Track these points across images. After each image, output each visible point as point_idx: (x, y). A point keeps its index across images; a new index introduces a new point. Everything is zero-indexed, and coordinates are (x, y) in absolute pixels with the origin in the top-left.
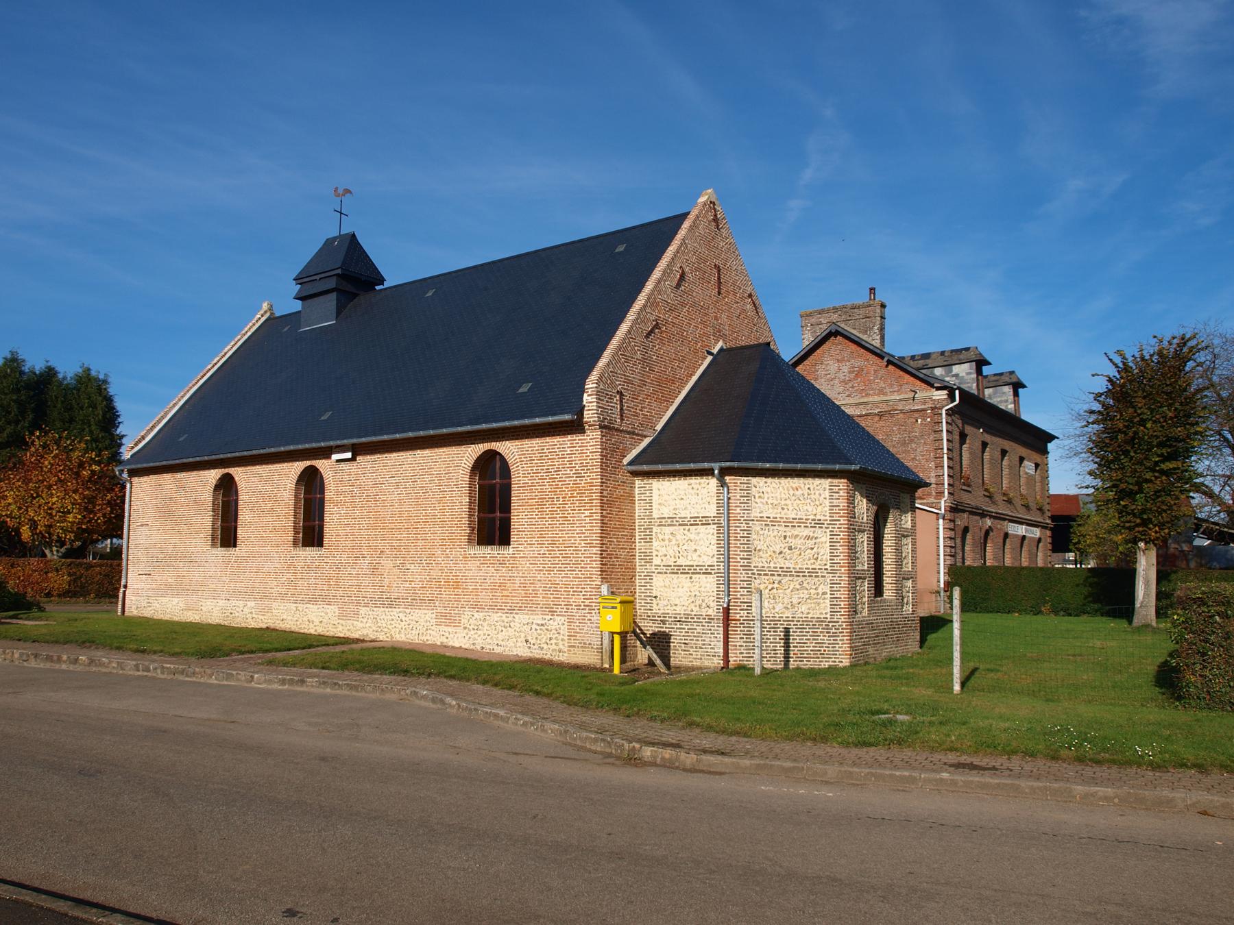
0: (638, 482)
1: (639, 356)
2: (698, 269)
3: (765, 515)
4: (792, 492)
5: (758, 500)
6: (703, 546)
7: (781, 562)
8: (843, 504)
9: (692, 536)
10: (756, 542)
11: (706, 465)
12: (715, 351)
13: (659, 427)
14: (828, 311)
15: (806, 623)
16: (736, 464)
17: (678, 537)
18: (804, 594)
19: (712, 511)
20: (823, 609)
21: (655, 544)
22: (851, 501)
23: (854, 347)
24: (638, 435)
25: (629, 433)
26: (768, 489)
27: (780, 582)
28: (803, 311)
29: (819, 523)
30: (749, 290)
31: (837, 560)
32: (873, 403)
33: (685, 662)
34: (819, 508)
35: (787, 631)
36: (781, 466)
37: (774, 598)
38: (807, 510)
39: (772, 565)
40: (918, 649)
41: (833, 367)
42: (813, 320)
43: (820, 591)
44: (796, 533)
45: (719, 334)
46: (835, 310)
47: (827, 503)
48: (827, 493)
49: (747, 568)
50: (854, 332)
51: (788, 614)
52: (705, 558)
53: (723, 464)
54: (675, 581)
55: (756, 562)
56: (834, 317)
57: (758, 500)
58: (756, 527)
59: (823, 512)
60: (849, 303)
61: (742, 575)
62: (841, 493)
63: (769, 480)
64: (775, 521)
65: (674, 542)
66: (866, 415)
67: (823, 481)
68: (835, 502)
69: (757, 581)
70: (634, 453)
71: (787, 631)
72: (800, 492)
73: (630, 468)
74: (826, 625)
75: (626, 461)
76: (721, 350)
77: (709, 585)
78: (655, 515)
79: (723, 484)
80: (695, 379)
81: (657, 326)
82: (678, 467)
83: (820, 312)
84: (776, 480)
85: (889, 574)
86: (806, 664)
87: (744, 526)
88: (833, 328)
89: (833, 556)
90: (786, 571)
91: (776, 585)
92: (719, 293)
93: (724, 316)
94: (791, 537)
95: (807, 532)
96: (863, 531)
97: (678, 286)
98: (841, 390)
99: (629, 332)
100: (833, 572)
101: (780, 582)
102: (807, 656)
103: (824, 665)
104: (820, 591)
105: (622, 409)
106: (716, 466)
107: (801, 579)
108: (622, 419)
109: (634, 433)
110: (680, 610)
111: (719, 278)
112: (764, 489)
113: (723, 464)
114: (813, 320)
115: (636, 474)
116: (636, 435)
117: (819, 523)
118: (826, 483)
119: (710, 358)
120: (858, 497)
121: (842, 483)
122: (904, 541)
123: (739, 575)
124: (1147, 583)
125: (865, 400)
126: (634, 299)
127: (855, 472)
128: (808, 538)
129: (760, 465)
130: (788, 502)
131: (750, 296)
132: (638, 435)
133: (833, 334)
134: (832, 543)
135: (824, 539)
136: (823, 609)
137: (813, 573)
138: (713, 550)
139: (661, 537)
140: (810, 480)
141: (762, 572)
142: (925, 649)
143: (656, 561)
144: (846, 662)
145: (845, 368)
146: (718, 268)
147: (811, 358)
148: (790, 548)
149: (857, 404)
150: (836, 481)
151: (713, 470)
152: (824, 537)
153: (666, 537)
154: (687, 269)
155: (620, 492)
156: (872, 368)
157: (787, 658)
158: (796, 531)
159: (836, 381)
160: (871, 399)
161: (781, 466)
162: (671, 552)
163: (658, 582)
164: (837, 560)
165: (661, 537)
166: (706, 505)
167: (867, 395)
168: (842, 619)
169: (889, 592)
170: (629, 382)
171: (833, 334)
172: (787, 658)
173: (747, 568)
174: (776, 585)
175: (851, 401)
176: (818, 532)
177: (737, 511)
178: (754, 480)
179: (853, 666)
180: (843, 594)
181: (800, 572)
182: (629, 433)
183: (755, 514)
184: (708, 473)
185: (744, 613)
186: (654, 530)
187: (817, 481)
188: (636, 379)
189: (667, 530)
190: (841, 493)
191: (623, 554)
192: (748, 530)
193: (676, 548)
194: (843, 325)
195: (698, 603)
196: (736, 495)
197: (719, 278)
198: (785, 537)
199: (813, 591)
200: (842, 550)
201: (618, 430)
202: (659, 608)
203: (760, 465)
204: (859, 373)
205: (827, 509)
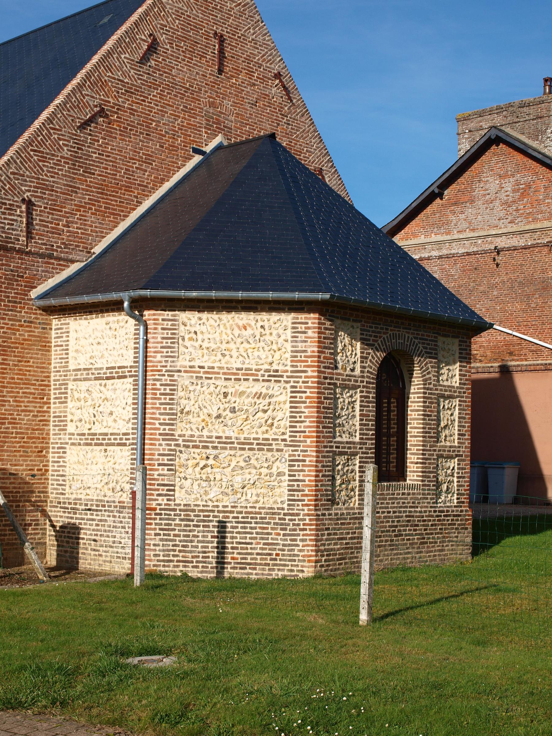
0: (55, 322)
1: (66, 152)
2: (184, 39)
3: (197, 363)
4: (237, 332)
5: (187, 343)
6: (117, 406)
7: (218, 430)
8: (312, 348)
9: (109, 394)
10: (183, 402)
11: (114, 296)
12: (208, 149)
13: (98, 249)
14: (491, 112)
15: (249, 516)
16: (148, 293)
17: (95, 395)
18: (250, 475)
19: (127, 358)
20: (279, 496)
21: (70, 404)
22: (327, 346)
23: (519, 157)
24: (58, 259)
25: (42, 256)
26: (203, 328)
27: (216, 457)
28: (459, 115)
29: (275, 376)
30: (276, 68)
31: (300, 427)
32: (542, 230)
33: (96, 567)
34: (277, 355)
35: (222, 526)
36: (213, 294)
37: (208, 480)
38: (260, 358)
39: (205, 433)
40: (463, 553)
41: (493, 184)
42: (472, 125)
43: (274, 470)
44: (241, 389)
45: (216, 125)
46: (500, 110)
47: (288, 346)
48: (289, 333)
49: (169, 437)
50: (523, 138)
51: (227, 501)
52: (121, 423)
53: (133, 293)
54: (90, 455)
55: (182, 428)
56: (498, 120)
57: (187, 343)
58: (184, 380)
59: (283, 360)
60: (517, 100)
61: (162, 447)
62: (310, 333)
63: (205, 315)
64: (210, 373)
65: (90, 402)
66: (533, 246)
67: (283, 316)
68: (301, 346)
69: (184, 456)
70: (51, 283)
71: (222, 526)
72: (249, 331)
73: (41, 303)
74: (281, 519)
75: (34, 294)
76: (219, 147)
77: (123, 458)
78: (71, 367)
79: (139, 319)
80: (167, 186)
81: (102, 113)
82: (86, 299)
83: (481, 114)
84: (215, 316)
85: (414, 450)
86: (238, 574)
87: (166, 379)
88: (493, 134)
89: (294, 421)
90: (226, 443)
91: (211, 462)
92: (220, 71)
93: (228, 104)
94: (234, 394)
95: (258, 387)
96: (355, 388)
97: (144, 59)
98: (502, 214)
99: (49, 120)
100: (294, 444)
101: (216, 457)
102: (250, 562)
103: (277, 574)
104: (274, 470)
105: (29, 224)
106: (125, 297)
107: (247, 453)
108: (29, 235)
109: (51, 256)
110: (93, 495)
111: (221, 51)
112: (197, 328)
113: (133, 293)
114: (472, 125)
115: (50, 310)
116: (52, 258)
117: (275, 376)
118: (287, 319)
119: (198, 158)
120: (344, 339)
121: (311, 319)
122: (345, 398)
123: (157, 448)
124: (433, 430)
125: (532, 226)
126: (69, 82)
127: (324, 302)
128: (259, 396)
129: (183, 294)
130: (232, 346)
131: (278, 76)
132: (58, 259)
133: (493, 140)
134: (294, 403)
135: (282, 398)
136: (279, 496)
137: (264, 445)
138: (128, 413)
139: (76, 395)
140: (264, 316)
141: (190, 443)
142: (483, 560)
143: (71, 428)
144: (308, 572)
145: (509, 186)
146: (221, 40)
147: (467, 175)
148: (233, 410)
149: (522, 233)
150: (302, 317)
151: (121, 302)
152: (282, 395)
153: (82, 396)
154: (162, 38)
155: (23, 334)
156: (541, 185)
157: (221, 563)
158: (243, 386)
159: (497, 203)
160: (539, 225)
161: (213, 294)
162: (86, 417)
163: (73, 455)
164: (300, 427)
165: (76, 395)
166: (124, 351)
167: (535, 220)
168: (305, 511)
169: (413, 475)
170: (45, 187)
171: (493, 140)
172: (221, 563)
173: (169, 437)
174: (211, 462)
175: (515, 228)
176: (275, 388)
177: (156, 358)
178: (183, 316)
179: (318, 576)
180: (308, 477)
181: (245, 444)
182: (42, 256)
183: (183, 362)
184: (115, 306)
185: (163, 501)
186: (70, 386)
187: (275, 317)
188: (60, 183)
189: (84, 385)
190: (310, 333)
191: (25, 418)
192: (173, 385)
193: (91, 411)
194: (508, 130)
195: (111, 486)
196: (156, 337)
197: (221, 51)
198: (225, 395)
199: (264, 471)
200: (308, 414)
201: (20, 252)
202: (72, 492)
203: (183, 294)
204: (524, 192)
205: (288, 355)
